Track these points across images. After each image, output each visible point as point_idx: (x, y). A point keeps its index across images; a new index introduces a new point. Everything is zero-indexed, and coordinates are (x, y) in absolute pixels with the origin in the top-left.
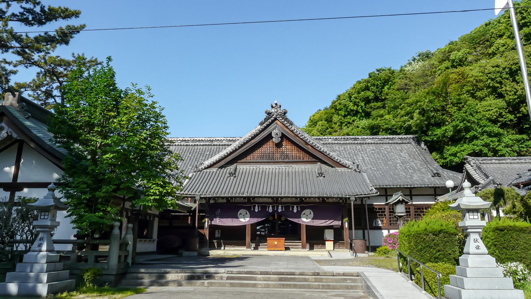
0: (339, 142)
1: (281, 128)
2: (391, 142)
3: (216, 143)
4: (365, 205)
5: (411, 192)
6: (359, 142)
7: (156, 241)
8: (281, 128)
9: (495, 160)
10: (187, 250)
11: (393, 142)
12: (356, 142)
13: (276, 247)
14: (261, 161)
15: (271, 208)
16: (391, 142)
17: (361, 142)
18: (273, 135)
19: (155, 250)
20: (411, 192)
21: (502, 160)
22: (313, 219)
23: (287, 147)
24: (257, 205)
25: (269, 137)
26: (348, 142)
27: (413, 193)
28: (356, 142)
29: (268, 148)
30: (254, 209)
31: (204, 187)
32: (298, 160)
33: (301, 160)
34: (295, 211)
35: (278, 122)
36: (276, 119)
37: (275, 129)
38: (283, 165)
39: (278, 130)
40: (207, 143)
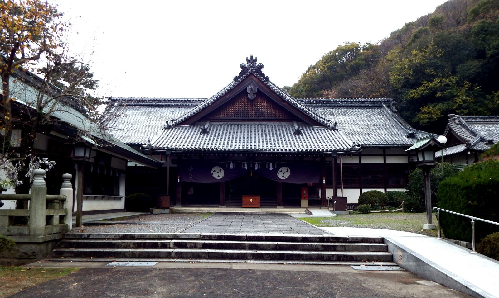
0: (311, 104)
1: (257, 83)
2: (362, 105)
3: (188, 104)
4: (340, 164)
5: (384, 152)
6: (331, 105)
7: (123, 199)
8: (257, 83)
9: (480, 118)
10: (158, 208)
11: (364, 105)
12: (328, 105)
13: (251, 204)
14: (236, 118)
15: (246, 165)
16: (362, 105)
17: (333, 105)
18: (248, 91)
19: (123, 207)
20: (384, 152)
21: (487, 118)
22: (420, 122)
23: (261, 106)
24: (232, 162)
25: (244, 92)
26: (319, 104)
27: (386, 154)
28: (328, 105)
29: (241, 105)
30: (229, 165)
31: (174, 139)
32: (273, 118)
33: (277, 118)
34: (271, 168)
35: (254, 78)
36: (251, 74)
37: (250, 84)
38: (258, 123)
39: (253, 86)
40: (179, 104)
